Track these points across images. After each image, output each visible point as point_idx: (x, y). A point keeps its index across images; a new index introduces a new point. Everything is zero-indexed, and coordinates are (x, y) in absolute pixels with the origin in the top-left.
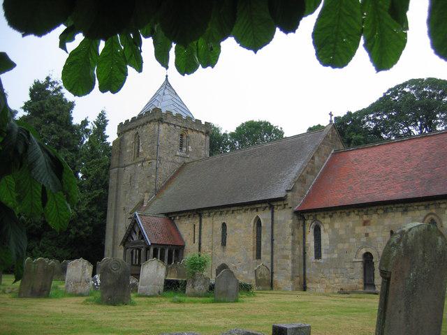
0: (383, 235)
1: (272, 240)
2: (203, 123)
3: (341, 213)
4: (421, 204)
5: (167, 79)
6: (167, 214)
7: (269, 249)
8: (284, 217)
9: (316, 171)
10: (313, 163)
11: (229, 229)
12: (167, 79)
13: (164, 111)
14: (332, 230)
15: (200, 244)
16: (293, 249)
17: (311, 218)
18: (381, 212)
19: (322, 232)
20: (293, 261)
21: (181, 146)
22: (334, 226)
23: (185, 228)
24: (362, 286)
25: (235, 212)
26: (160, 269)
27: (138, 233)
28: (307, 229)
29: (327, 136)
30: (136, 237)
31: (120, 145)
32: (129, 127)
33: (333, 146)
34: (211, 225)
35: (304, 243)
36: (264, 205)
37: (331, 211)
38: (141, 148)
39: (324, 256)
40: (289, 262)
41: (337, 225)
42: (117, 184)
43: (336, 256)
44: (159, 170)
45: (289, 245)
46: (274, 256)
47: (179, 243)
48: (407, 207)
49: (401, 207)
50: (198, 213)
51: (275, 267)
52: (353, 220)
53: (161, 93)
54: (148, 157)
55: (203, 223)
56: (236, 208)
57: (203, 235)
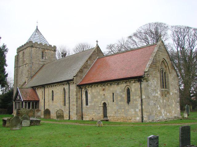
0: (110, 95)
1: (69, 98)
2: (53, 46)
5: (37, 28)
6: (32, 87)
8: (73, 87)
9: (89, 67)
11: (54, 93)
12: (37, 28)
13: (34, 42)
15: (44, 100)
16: (77, 101)
20: (77, 107)
21: (43, 57)
23: (39, 92)
25: (56, 86)
28: (83, 92)
29: (95, 51)
30: (18, 98)
31: (17, 58)
33: (98, 55)
34: (48, 91)
35: (82, 98)
36: (66, 83)
37: (91, 84)
39: (89, 104)
40: (75, 107)
41: (93, 91)
43: (93, 104)
44: (32, 68)
46: (70, 104)
48: (119, 82)
50: (43, 86)
51: (70, 109)
52: (99, 88)
53: (34, 34)
55: (45, 91)
57: (45, 96)
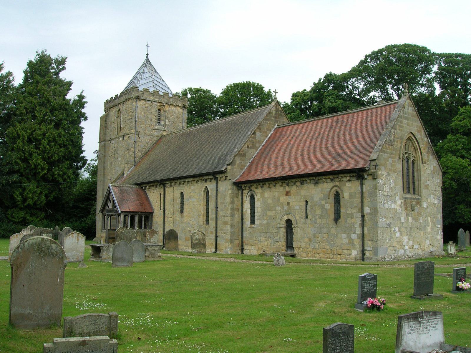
1: (217, 208)
3: (269, 184)
4: (327, 177)
5: (147, 57)
6: (139, 184)
7: (214, 216)
8: (226, 187)
9: (257, 145)
10: (255, 138)
12: (147, 57)
14: (263, 199)
15: (164, 211)
16: (232, 216)
17: (247, 188)
18: (298, 184)
19: (256, 200)
20: (232, 226)
21: (159, 120)
22: (264, 196)
23: (154, 195)
24: (284, 248)
25: (190, 183)
26: (80, 240)
27: (112, 202)
28: (244, 197)
30: (110, 205)
32: (113, 104)
33: (277, 122)
34: (173, 192)
36: (210, 177)
38: (122, 123)
39: (257, 222)
40: (229, 227)
41: (266, 195)
42: (105, 156)
43: (265, 222)
45: (229, 213)
47: (148, 210)
49: (313, 179)
50: (162, 183)
51: (218, 231)
53: (141, 71)
54: (128, 132)
55: (166, 192)
56: (190, 179)
57: (166, 203)
